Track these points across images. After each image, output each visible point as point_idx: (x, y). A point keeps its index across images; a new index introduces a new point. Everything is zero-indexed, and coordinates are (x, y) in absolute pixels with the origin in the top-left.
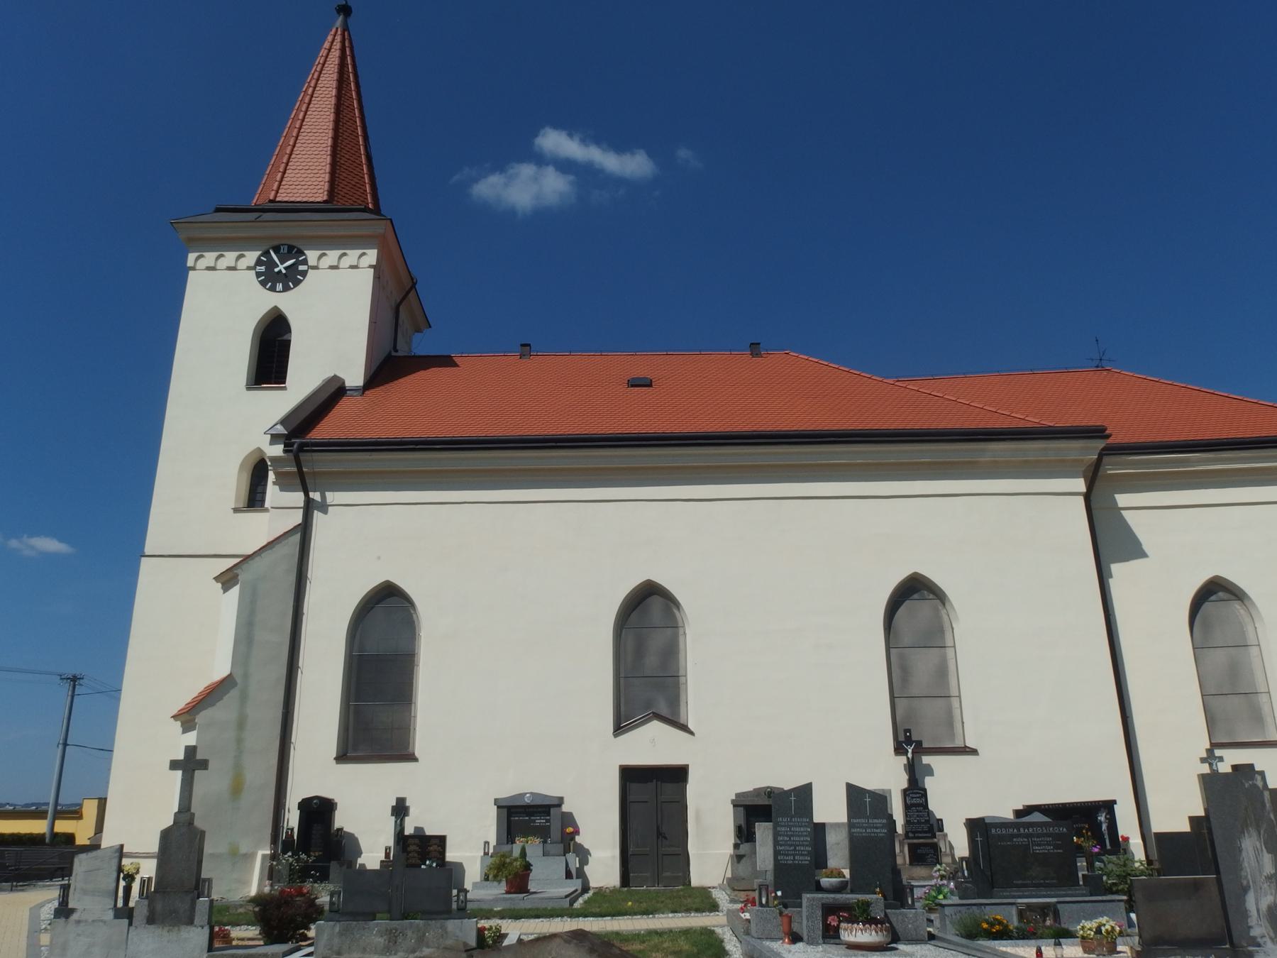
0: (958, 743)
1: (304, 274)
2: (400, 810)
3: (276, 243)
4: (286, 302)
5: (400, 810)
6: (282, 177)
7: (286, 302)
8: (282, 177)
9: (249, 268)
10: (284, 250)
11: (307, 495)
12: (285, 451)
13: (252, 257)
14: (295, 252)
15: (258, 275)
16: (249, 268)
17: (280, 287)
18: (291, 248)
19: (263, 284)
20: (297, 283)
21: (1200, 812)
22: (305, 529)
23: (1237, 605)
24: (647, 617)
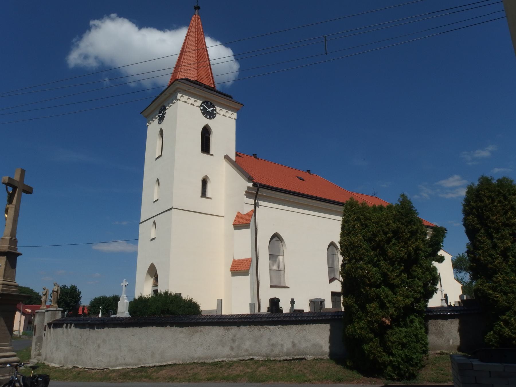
0: (283, 285)
1: (215, 114)
2: (293, 302)
3: (207, 100)
4: (211, 123)
5: (293, 302)
6: (213, 82)
7: (211, 123)
8: (213, 82)
9: (198, 106)
10: (209, 103)
11: (255, 201)
12: (253, 185)
13: (199, 102)
14: (212, 105)
15: (201, 110)
16: (198, 106)
17: (208, 117)
18: (211, 104)
19: (214, 117)
20: (203, 114)
21: (305, 311)
22: (255, 211)
23: (280, 242)
24: (154, 223)
